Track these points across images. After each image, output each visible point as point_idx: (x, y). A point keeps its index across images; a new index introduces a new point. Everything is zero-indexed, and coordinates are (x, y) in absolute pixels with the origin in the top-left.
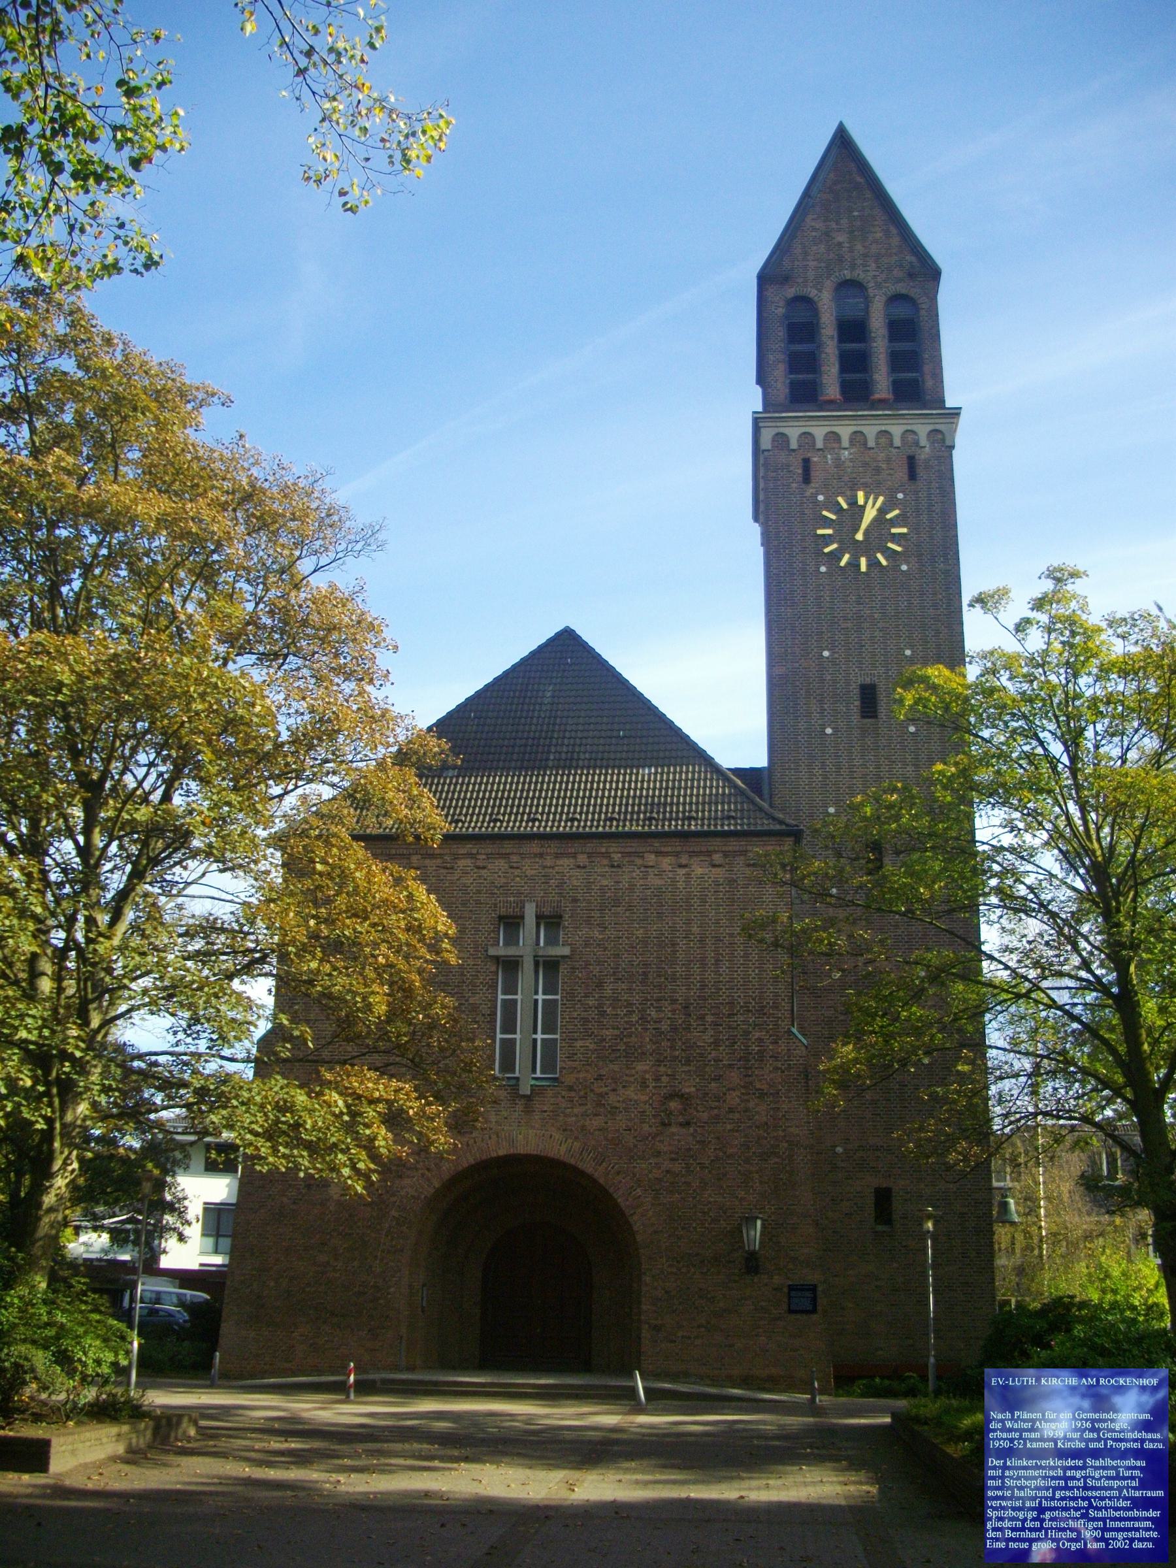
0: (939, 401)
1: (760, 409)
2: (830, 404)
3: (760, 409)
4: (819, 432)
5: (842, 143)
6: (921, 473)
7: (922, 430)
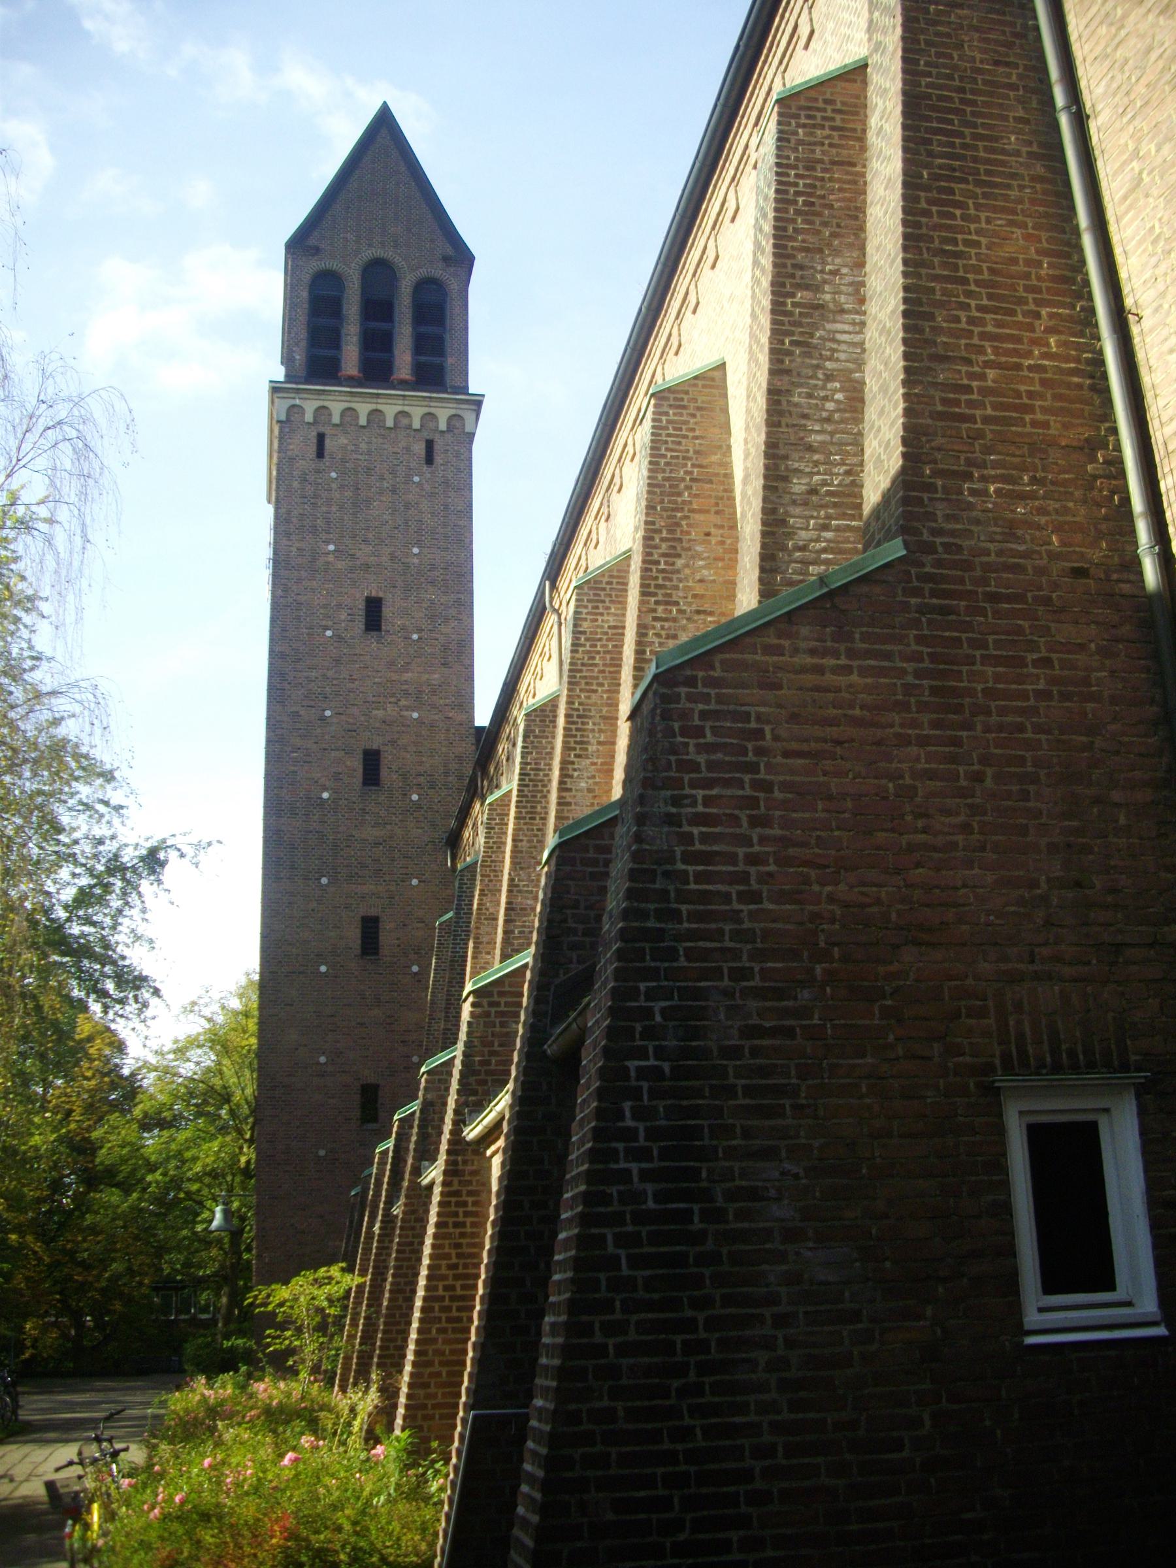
0: (464, 389)
1: (282, 379)
2: (403, 384)
3: (282, 379)
4: (336, 408)
5: (383, 133)
6: (438, 459)
7: (443, 416)
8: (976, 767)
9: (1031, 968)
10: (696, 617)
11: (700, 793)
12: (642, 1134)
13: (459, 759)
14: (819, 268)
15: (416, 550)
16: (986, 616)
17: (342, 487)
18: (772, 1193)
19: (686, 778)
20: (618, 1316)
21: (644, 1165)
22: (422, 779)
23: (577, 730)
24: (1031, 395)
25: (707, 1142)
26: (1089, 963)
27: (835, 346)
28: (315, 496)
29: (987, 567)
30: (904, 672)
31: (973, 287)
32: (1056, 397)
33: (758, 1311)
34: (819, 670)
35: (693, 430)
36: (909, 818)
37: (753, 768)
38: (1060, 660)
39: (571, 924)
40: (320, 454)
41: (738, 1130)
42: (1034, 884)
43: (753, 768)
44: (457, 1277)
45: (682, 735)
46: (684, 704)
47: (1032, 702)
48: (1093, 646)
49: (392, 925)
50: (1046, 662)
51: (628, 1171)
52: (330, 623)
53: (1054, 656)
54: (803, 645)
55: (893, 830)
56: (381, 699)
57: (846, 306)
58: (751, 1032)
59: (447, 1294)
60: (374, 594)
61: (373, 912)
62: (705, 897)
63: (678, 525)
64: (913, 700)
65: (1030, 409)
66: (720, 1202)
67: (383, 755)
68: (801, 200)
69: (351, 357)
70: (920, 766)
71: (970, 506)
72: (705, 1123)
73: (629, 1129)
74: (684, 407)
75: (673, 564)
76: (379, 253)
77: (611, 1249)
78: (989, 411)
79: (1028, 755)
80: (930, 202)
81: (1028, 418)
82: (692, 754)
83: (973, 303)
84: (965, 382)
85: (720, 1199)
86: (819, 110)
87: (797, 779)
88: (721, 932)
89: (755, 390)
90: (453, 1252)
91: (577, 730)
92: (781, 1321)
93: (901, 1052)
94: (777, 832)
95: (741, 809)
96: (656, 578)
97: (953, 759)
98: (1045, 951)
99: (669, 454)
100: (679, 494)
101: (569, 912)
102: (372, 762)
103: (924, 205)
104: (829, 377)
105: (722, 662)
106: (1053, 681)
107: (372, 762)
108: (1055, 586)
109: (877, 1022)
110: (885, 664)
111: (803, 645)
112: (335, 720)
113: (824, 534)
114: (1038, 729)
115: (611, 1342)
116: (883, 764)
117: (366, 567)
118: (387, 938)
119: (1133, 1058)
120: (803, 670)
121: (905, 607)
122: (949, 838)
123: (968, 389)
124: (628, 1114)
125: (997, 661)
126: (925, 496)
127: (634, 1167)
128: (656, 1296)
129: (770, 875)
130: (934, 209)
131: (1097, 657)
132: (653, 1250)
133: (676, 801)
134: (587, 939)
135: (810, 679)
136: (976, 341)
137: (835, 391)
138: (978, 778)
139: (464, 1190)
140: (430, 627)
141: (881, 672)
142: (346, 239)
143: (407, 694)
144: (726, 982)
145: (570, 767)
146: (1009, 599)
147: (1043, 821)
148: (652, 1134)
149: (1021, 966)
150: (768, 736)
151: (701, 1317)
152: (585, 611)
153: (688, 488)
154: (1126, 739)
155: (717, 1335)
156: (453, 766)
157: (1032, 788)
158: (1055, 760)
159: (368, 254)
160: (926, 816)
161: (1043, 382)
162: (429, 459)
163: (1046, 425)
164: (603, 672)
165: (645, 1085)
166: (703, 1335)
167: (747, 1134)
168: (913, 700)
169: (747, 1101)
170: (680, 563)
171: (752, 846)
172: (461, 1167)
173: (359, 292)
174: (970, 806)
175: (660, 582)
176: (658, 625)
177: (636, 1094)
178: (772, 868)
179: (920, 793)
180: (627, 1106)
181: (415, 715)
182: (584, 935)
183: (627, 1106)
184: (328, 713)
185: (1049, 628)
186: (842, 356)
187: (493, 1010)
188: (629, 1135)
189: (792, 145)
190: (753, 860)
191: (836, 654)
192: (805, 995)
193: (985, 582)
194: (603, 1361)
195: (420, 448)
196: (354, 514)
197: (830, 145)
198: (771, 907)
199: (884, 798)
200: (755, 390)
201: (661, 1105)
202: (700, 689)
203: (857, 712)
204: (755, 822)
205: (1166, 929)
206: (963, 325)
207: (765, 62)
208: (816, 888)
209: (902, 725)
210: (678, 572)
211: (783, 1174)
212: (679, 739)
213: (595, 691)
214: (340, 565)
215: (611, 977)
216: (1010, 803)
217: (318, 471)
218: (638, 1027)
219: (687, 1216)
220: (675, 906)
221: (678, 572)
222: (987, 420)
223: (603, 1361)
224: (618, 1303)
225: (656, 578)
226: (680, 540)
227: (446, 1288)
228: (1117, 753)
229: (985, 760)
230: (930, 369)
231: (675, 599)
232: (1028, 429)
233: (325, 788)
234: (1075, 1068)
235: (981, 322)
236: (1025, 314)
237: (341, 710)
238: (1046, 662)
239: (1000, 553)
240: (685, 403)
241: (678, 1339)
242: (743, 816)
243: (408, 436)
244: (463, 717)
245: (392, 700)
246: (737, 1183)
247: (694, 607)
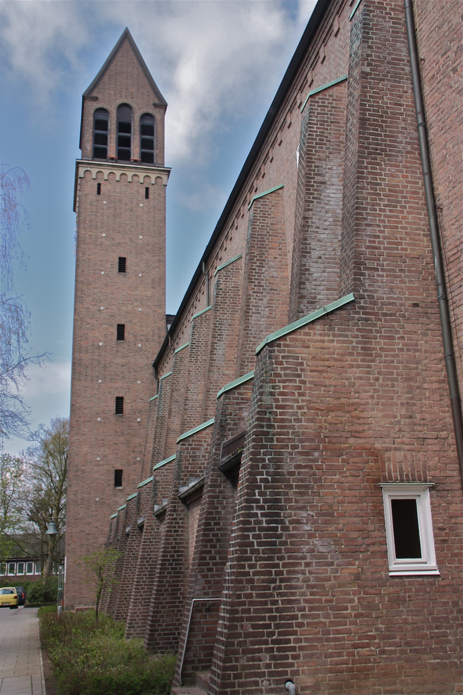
6: (151, 196)
8: (377, 376)
9: (394, 446)
10: (270, 292)
11: (281, 384)
12: (261, 501)
13: (159, 329)
14: (324, 167)
15: (141, 237)
16: (381, 322)
17: (109, 208)
18: (305, 521)
19: (277, 379)
20: (253, 562)
21: (262, 511)
22: (143, 338)
23: (219, 330)
24: (401, 239)
25: (283, 504)
26: (414, 444)
27: (329, 199)
28: (97, 212)
29: (383, 304)
30: (352, 342)
31: (382, 197)
32: (411, 239)
33: (300, 561)
34: (323, 341)
35: (270, 214)
36: (352, 393)
37: (299, 376)
38: (408, 337)
39: (229, 421)
40: (99, 192)
41: (293, 500)
42: (395, 417)
43: (299, 376)
44: (175, 552)
45: (276, 364)
46: (276, 353)
47: (397, 352)
48: (419, 332)
49: (129, 401)
50: (403, 338)
51: (257, 513)
52: (103, 268)
53: (405, 336)
54: (317, 332)
55: (347, 398)
56: (125, 302)
57: (334, 183)
58: (298, 467)
59: (171, 558)
60: (122, 256)
61: (121, 395)
62: (283, 420)
63: (263, 254)
64: (355, 352)
65: (401, 244)
66: (287, 524)
67: (126, 327)
68: (318, 138)
69: (112, 149)
70: (357, 375)
71: (377, 281)
72: (283, 497)
73: (257, 499)
74: (267, 205)
75: (261, 270)
76: (125, 101)
77: (251, 539)
78: (386, 245)
79: (395, 371)
80: (368, 163)
81: (400, 247)
82: (279, 371)
83: (382, 203)
84: (378, 234)
85: (287, 523)
86: (327, 99)
87: (314, 380)
88: (288, 433)
89: (299, 215)
90: (174, 542)
91: (219, 330)
92: (307, 565)
93: (348, 474)
94: (308, 398)
95: (295, 390)
96: (255, 276)
97: (368, 373)
98: (399, 440)
99: (260, 224)
100: (264, 241)
101: (228, 417)
102: (121, 329)
103: (365, 164)
104: (327, 212)
105: (290, 338)
106: (405, 345)
107: (121, 329)
108: (406, 310)
109: (340, 463)
110: (346, 339)
111: (317, 332)
112: (105, 311)
113: (324, 274)
114: (399, 362)
115: (251, 571)
116: (344, 374)
117: (119, 244)
118: (127, 407)
119: (429, 478)
120: (317, 341)
121: (353, 318)
122: (366, 400)
123: (378, 237)
124: (257, 494)
125: (386, 338)
126: (362, 278)
127: (259, 512)
128: (266, 555)
129: (305, 413)
130: (369, 166)
131: (421, 336)
132: (265, 540)
133: (274, 387)
134: (234, 427)
135: (319, 344)
136: (382, 218)
137: (330, 217)
138: (377, 379)
139: (178, 517)
140: (147, 271)
141: (344, 342)
142: (109, 93)
143: (136, 300)
144: (290, 450)
145: (216, 345)
146: (391, 315)
147: (399, 394)
148: (265, 501)
149: (390, 445)
150: (305, 365)
151: (281, 563)
152: (222, 280)
153: (268, 239)
154: (430, 365)
155: (286, 569)
156: (157, 332)
157: (395, 383)
158: (404, 373)
159: (120, 101)
160: (358, 392)
161: (406, 233)
162: (147, 197)
163: (406, 250)
164: (229, 306)
165: (263, 484)
166: (281, 569)
167: (296, 501)
168: (355, 352)
169: (296, 490)
170: (264, 269)
171: (299, 403)
172: (177, 508)
173: (116, 119)
174: (374, 389)
175: (256, 277)
176: (255, 294)
177: (260, 487)
178: (305, 410)
179: (357, 385)
180: (257, 491)
181: (140, 309)
182: (233, 425)
183: (257, 491)
184: (102, 308)
185: (404, 325)
186: (332, 203)
187: (190, 447)
188: (257, 501)
189: (316, 115)
190: (300, 408)
191: (329, 335)
192: (316, 454)
193: (382, 309)
194: (248, 577)
195: (143, 191)
196: (114, 220)
197: (331, 114)
198: (305, 424)
199: (345, 386)
200: (299, 215)
201: (268, 491)
202: (282, 348)
203: (335, 356)
204: (300, 395)
205: (442, 433)
206: (378, 212)
207: (304, 64)
208: (320, 417)
209: (351, 361)
210: (264, 273)
211: (308, 515)
212: (275, 366)
213: (226, 314)
214: (107, 243)
215: (251, 447)
216: (387, 388)
217: (98, 201)
218: (260, 465)
219: (276, 529)
220: (273, 423)
221: (264, 273)
222: (385, 248)
223: (248, 577)
224: (253, 558)
225: (255, 276)
226: (264, 261)
227: (171, 556)
228: (426, 370)
229: (379, 373)
230: (365, 229)
231: (262, 284)
232: (400, 252)
233: (100, 341)
234: (408, 481)
235: (384, 211)
236: (401, 207)
237: (108, 307)
238: (403, 338)
239: (387, 298)
240: (267, 203)
241: (273, 570)
242: (296, 392)
243: (138, 186)
244: (161, 311)
245: (130, 303)
246: (293, 518)
247: (270, 288)
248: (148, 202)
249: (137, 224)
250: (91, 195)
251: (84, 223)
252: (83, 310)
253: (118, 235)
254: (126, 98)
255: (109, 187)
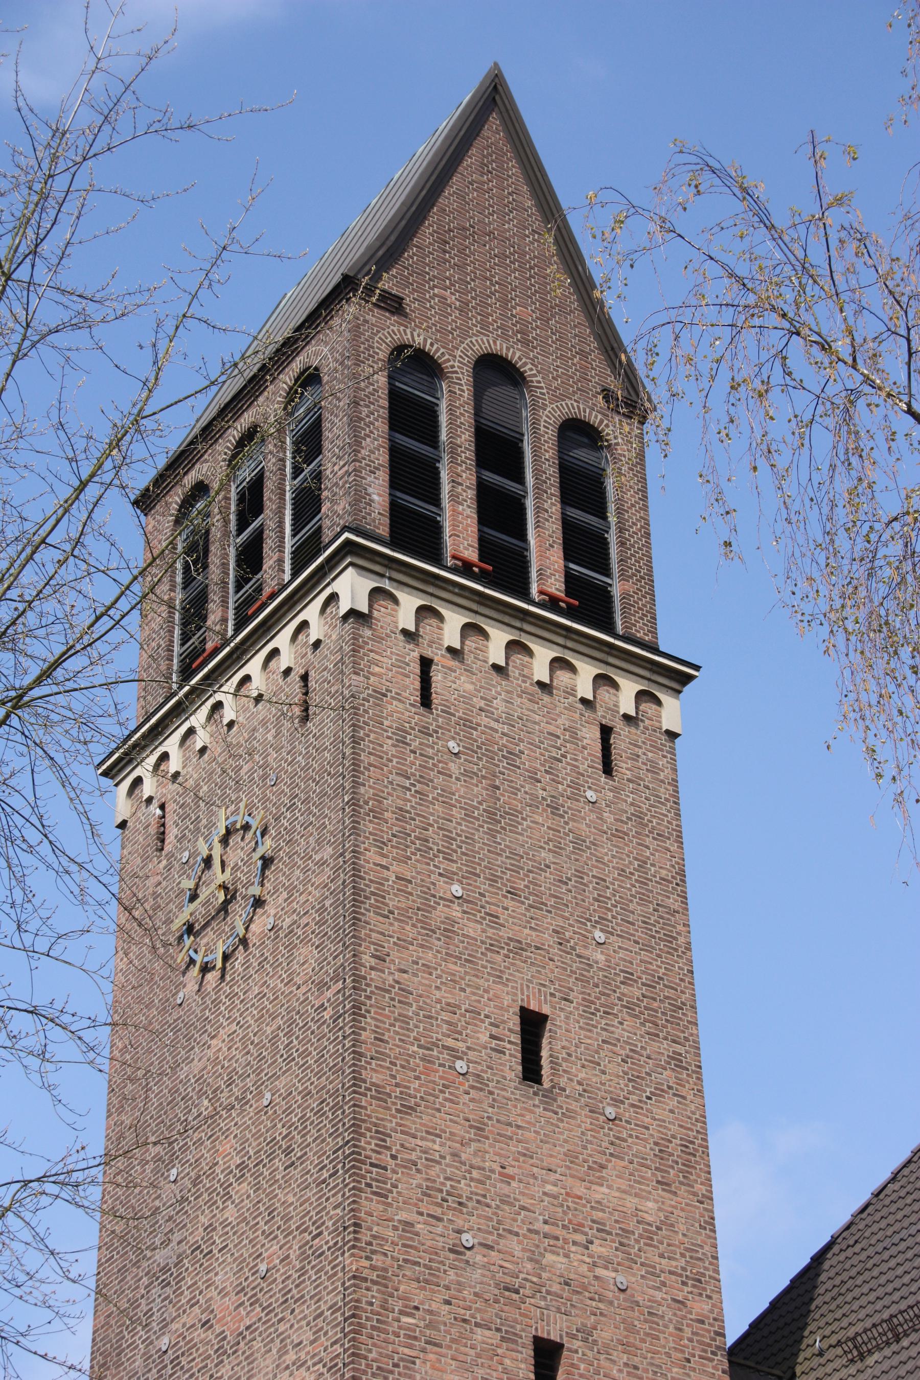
6: (622, 766)
17: (468, 774)
56: (559, 1232)
60: (533, 1006)
117: (518, 948)
237: (490, 1239)
248: (614, 790)
249: (580, 874)
250: (398, 698)
251: (377, 814)
252: (390, 1233)
253: (508, 903)
254: (505, 337)
255: (465, 684)
